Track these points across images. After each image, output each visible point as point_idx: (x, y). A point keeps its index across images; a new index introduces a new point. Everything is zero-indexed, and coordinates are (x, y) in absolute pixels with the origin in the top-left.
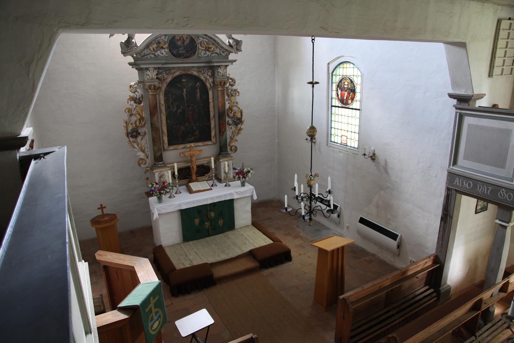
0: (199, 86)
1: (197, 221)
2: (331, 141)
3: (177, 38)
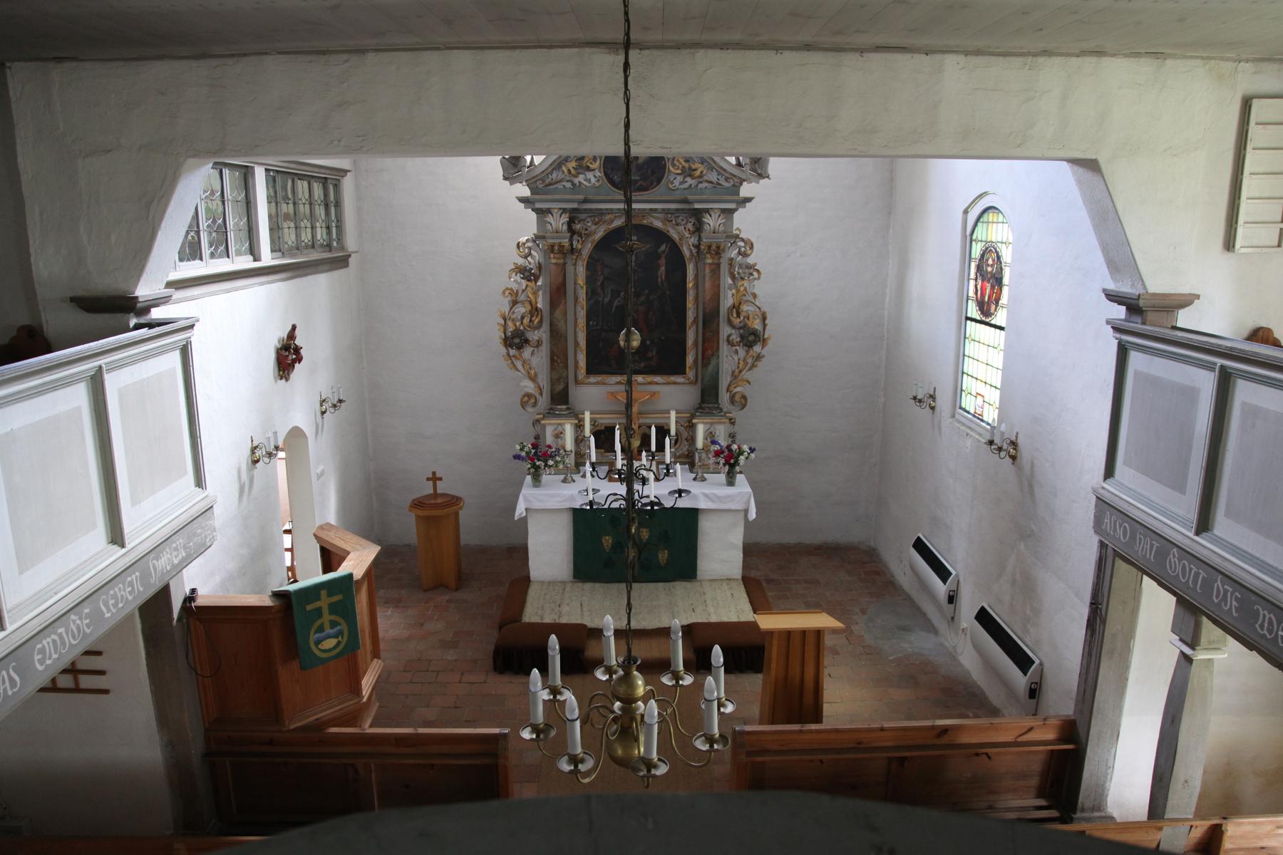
0: (666, 252)
1: (607, 541)
2: (961, 408)
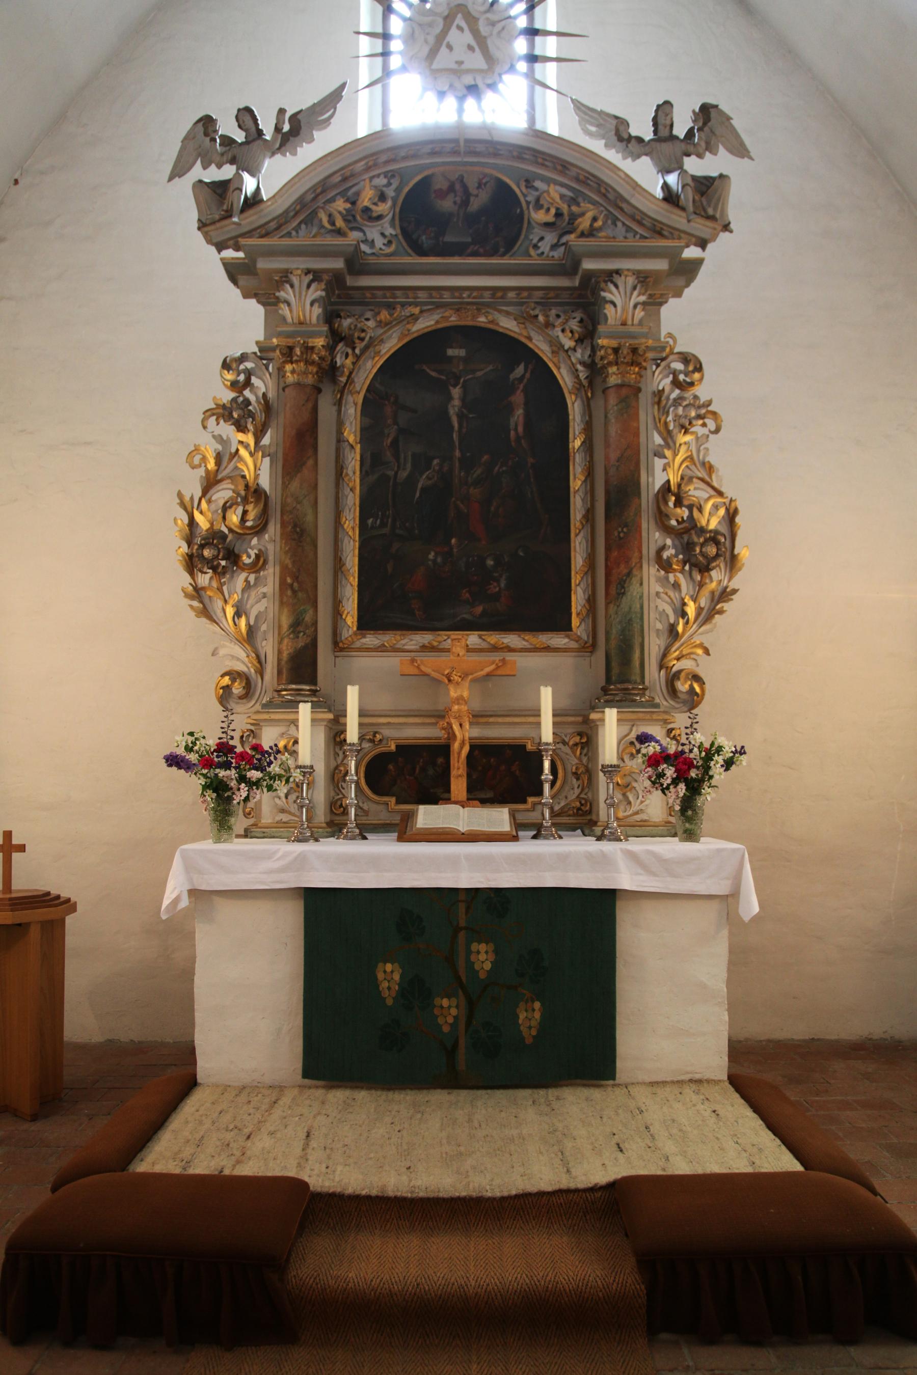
0: (525, 380)
3: (440, 184)
